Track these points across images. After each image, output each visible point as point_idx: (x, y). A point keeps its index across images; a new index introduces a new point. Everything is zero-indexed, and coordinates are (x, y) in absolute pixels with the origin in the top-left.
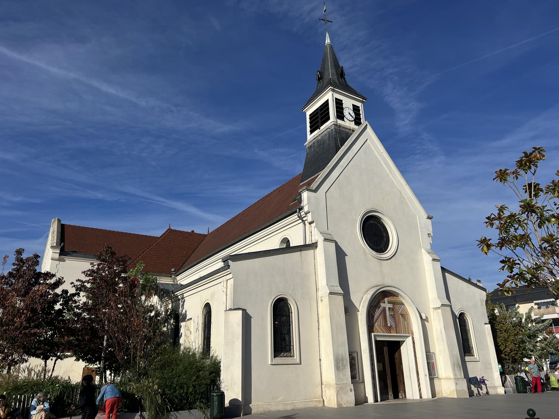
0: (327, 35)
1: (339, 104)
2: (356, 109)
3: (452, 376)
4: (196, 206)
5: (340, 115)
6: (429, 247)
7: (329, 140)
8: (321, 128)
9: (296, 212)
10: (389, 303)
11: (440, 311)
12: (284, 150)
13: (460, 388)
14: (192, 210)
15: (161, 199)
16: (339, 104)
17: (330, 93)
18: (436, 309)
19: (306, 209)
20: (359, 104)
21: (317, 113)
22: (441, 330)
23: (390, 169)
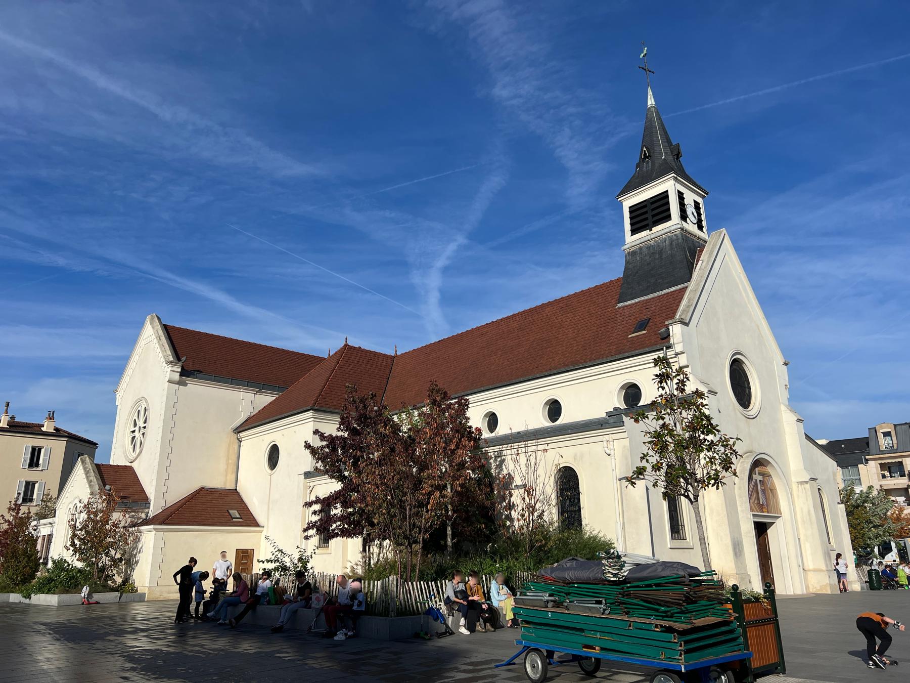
0: (650, 92)
1: (681, 196)
2: (697, 206)
3: (824, 568)
4: (230, 291)
5: (684, 216)
6: (787, 403)
7: (672, 249)
8: (655, 229)
9: (662, 349)
10: (760, 474)
11: (807, 486)
12: (393, 215)
13: (832, 582)
14: (220, 297)
15: (170, 275)
16: (681, 196)
17: (672, 182)
18: (802, 483)
19: (678, 348)
20: (699, 200)
21: (645, 206)
22: (809, 511)
23: (748, 296)
